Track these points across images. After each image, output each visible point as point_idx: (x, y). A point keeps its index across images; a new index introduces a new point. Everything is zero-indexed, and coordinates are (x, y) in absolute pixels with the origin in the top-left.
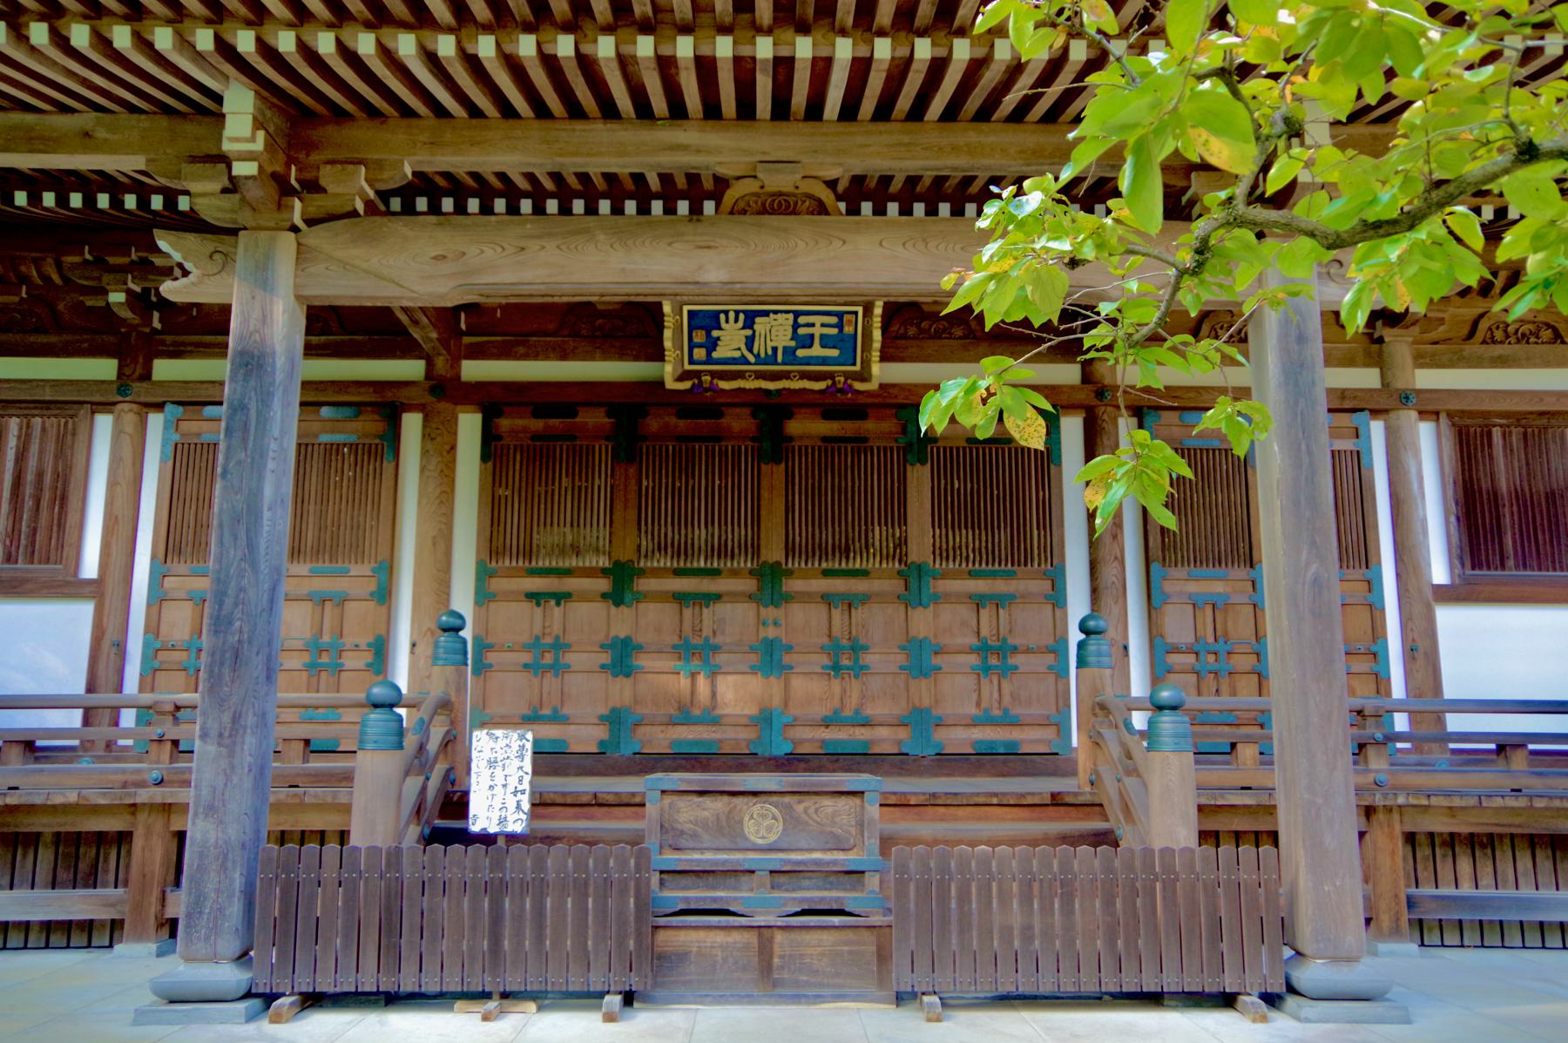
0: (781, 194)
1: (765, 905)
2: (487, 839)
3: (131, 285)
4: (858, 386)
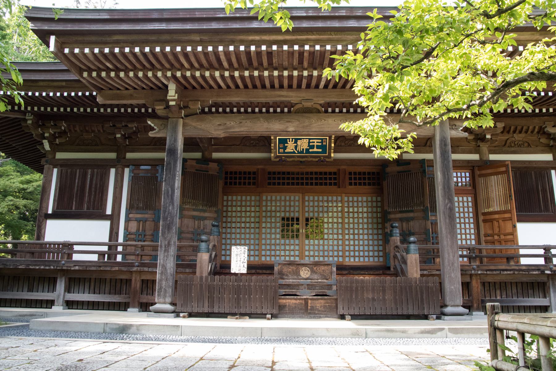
0: (308, 108)
1: (307, 294)
2: (235, 274)
3: (51, 131)
4: (327, 160)
